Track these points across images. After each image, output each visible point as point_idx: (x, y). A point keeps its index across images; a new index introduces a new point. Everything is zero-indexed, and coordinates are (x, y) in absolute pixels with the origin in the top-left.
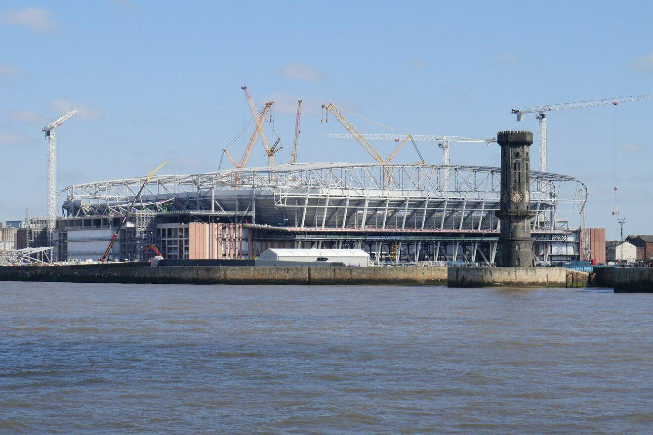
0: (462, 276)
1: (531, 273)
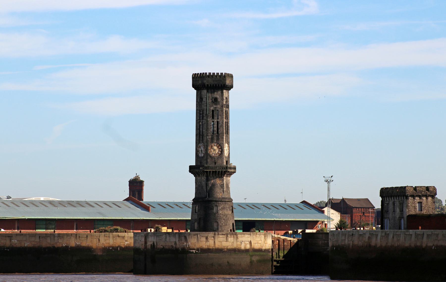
0: (152, 243)
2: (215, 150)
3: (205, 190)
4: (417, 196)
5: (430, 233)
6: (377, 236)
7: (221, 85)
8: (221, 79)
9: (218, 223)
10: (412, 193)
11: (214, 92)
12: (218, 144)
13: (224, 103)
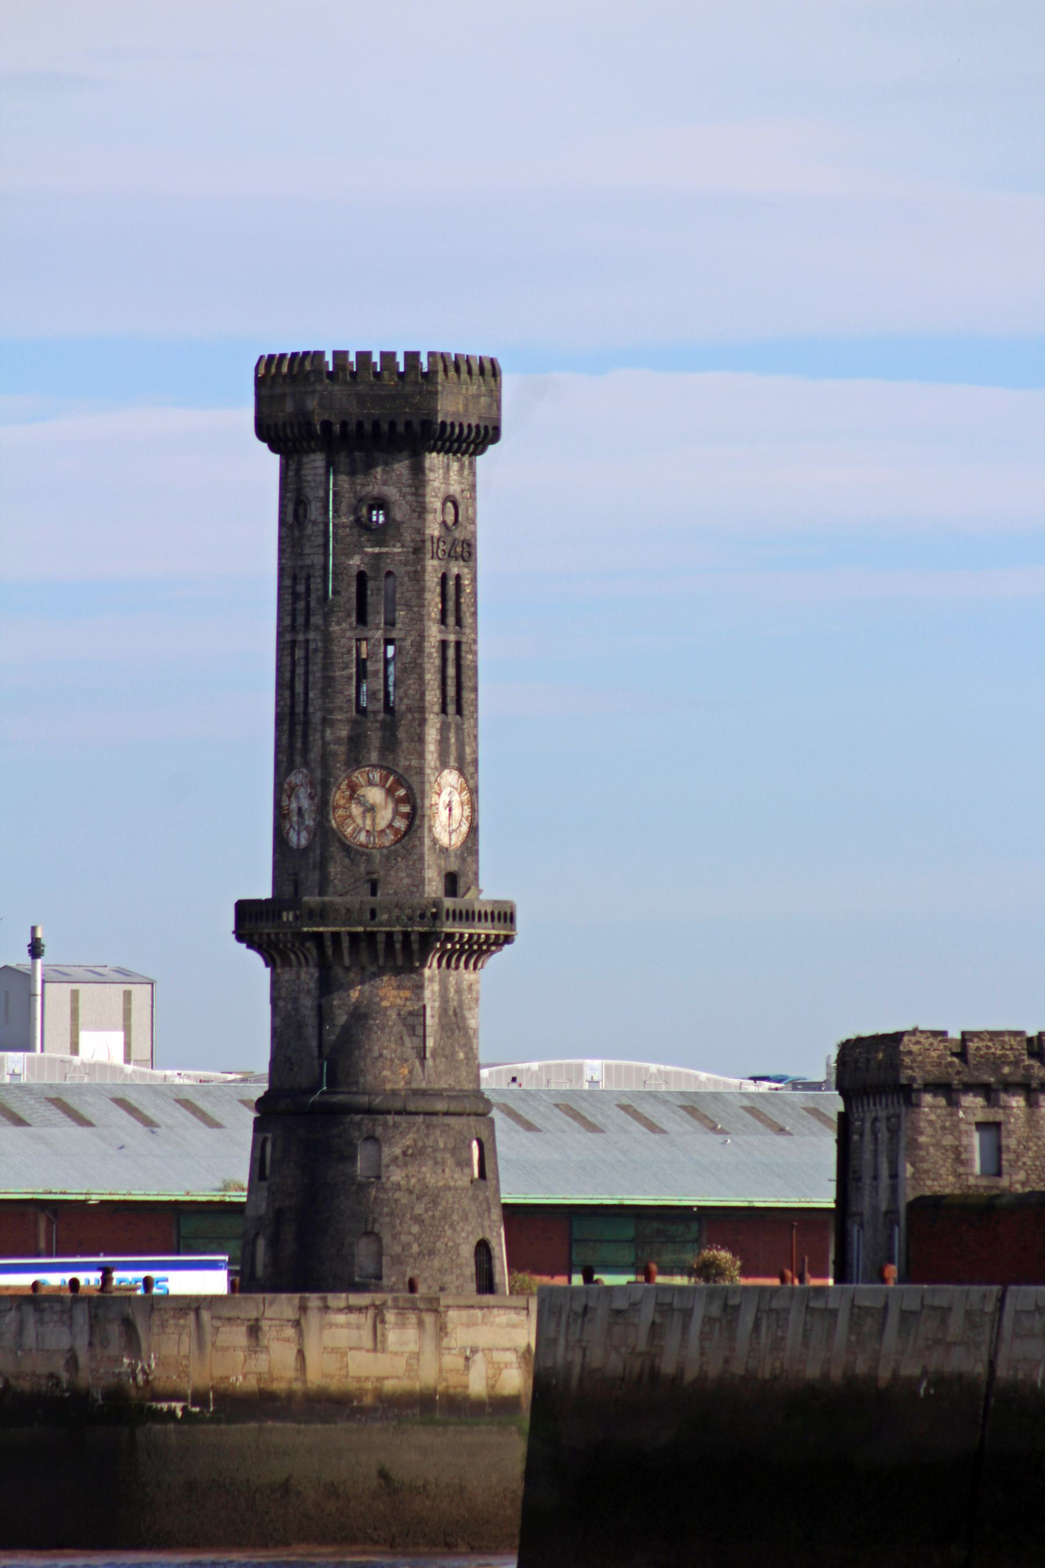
1: (411, 1333)
2: (370, 809)
3: (314, 1043)
4: (969, 1088)
5: (913, 1305)
6: (687, 1314)
7: (408, 424)
8: (408, 389)
9: (378, 1239)
10: (935, 1074)
11: (369, 466)
12: (391, 771)
13: (434, 529)
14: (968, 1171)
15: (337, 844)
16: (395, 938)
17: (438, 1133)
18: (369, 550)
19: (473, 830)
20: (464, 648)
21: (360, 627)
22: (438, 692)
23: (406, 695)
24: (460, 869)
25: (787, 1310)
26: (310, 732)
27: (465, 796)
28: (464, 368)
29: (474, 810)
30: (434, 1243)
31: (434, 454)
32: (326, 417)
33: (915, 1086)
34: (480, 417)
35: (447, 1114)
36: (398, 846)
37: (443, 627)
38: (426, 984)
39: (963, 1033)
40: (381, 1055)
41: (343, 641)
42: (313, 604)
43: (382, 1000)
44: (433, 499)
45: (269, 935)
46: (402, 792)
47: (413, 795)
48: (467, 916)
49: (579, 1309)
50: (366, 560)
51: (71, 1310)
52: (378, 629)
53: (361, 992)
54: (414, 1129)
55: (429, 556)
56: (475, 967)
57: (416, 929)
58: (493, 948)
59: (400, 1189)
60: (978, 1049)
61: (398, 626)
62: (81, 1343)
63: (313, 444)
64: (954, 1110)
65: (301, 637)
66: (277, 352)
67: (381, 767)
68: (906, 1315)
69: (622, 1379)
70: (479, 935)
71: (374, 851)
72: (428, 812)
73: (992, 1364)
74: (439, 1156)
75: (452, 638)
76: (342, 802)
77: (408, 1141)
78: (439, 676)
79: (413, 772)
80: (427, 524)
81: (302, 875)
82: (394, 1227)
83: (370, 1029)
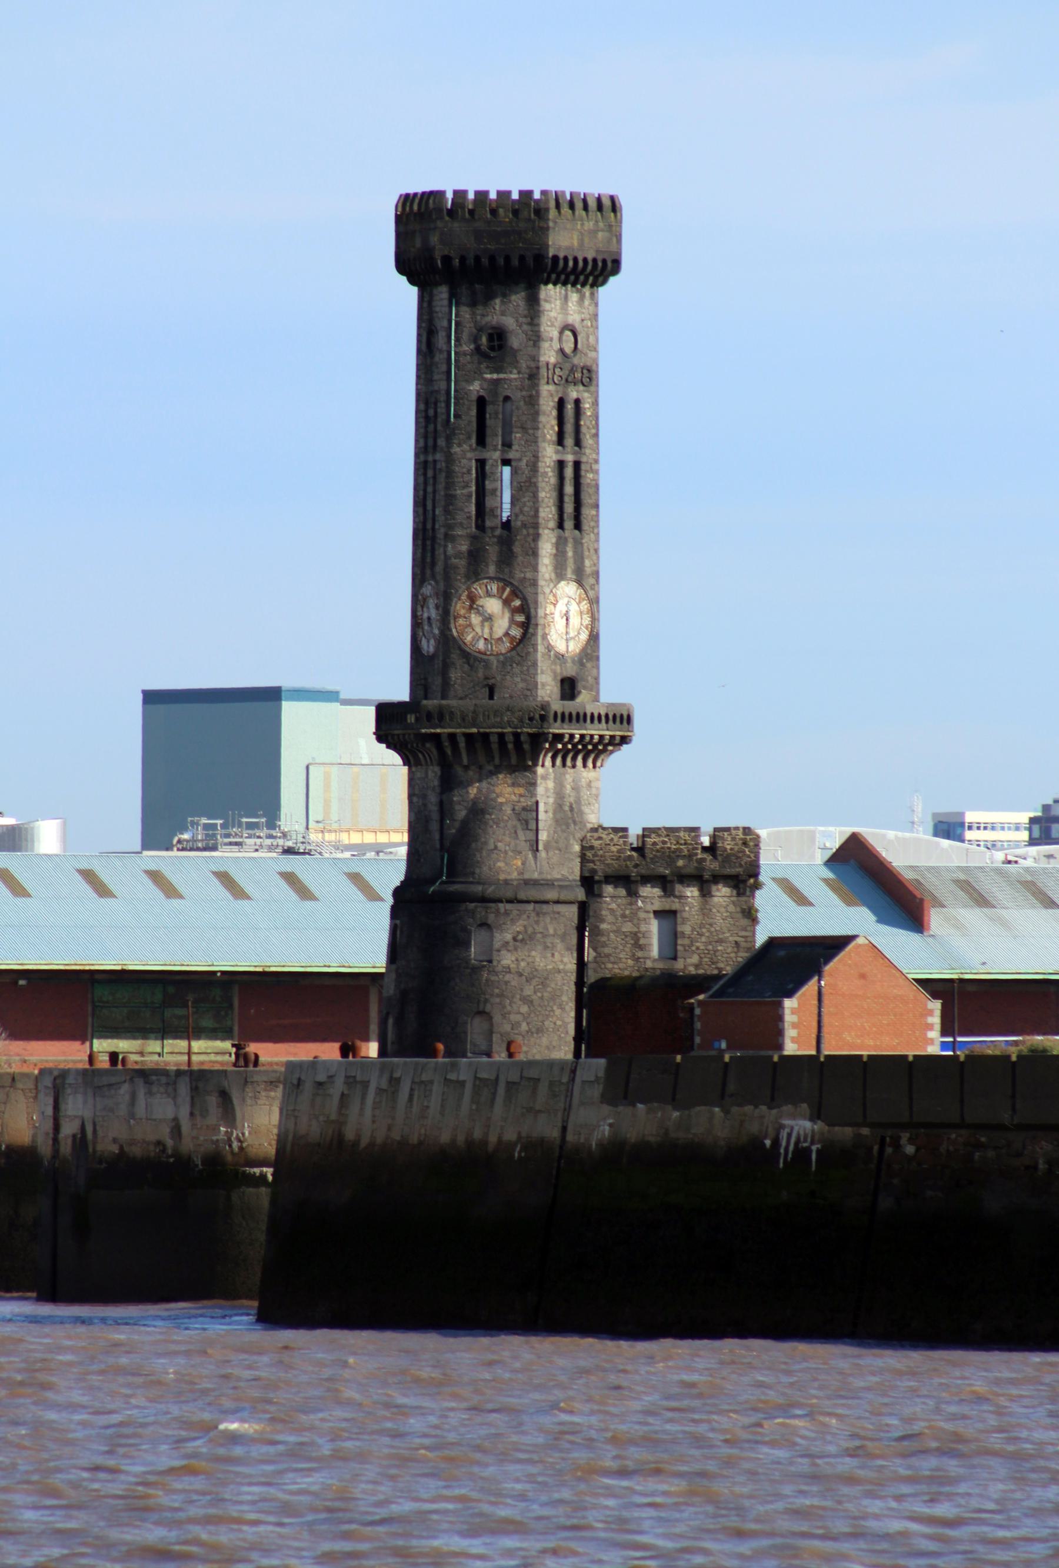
2: (489, 619)
3: (437, 836)
4: (646, 879)
6: (366, 1085)
7: (522, 258)
8: (522, 225)
9: (491, 1018)
11: (489, 298)
12: (507, 583)
13: (549, 355)
14: (646, 955)
15: (458, 652)
16: (507, 739)
17: (548, 920)
18: (488, 376)
19: (594, 638)
20: (583, 467)
21: (479, 448)
22: (554, 509)
23: (521, 511)
24: (577, 674)
25: (431, 1082)
26: (437, 546)
27: (585, 606)
28: (579, 205)
29: (594, 619)
30: (543, 1022)
31: (550, 286)
32: (446, 253)
33: (597, 878)
34: (598, 251)
35: (558, 902)
36: (514, 653)
37: (560, 448)
38: (539, 782)
39: (644, 829)
40: (496, 848)
41: (464, 461)
42: (439, 427)
43: (498, 796)
44: (548, 329)
45: (398, 735)
46: (517, 603)
47: (528, 605)
48: (580, 718)
49: (295, 1082)
50: (485, 386)
51: (175, 1083)
52: (495, 450)
53: (479, 790)
54: (525, 916)
55: (543, 381)
56: (594, 767)
57: (525, 730)
58: (610, 748)
59: (510, 972)
60: (655, 844)
61: (515, 447)
62: (184, 1112)
63: (437, 277)
64: (634, 899)
65: (430, 458)
66: (411, 191)
67: (499, 579)
68: (510, 1085)
69: (319, 1144)
70: (592, 736)
71: (491, 658)
72: (541, 621)
73: (564, 1129)
74: (548, 940)
75: (570, 458)
76: (462, 612)
77: (518, 927)
78: (555, 494)
79: (528, 583)
80: (542, 352)
81: (430, 680)
82: (504, 1007)
83: (486, 823)
